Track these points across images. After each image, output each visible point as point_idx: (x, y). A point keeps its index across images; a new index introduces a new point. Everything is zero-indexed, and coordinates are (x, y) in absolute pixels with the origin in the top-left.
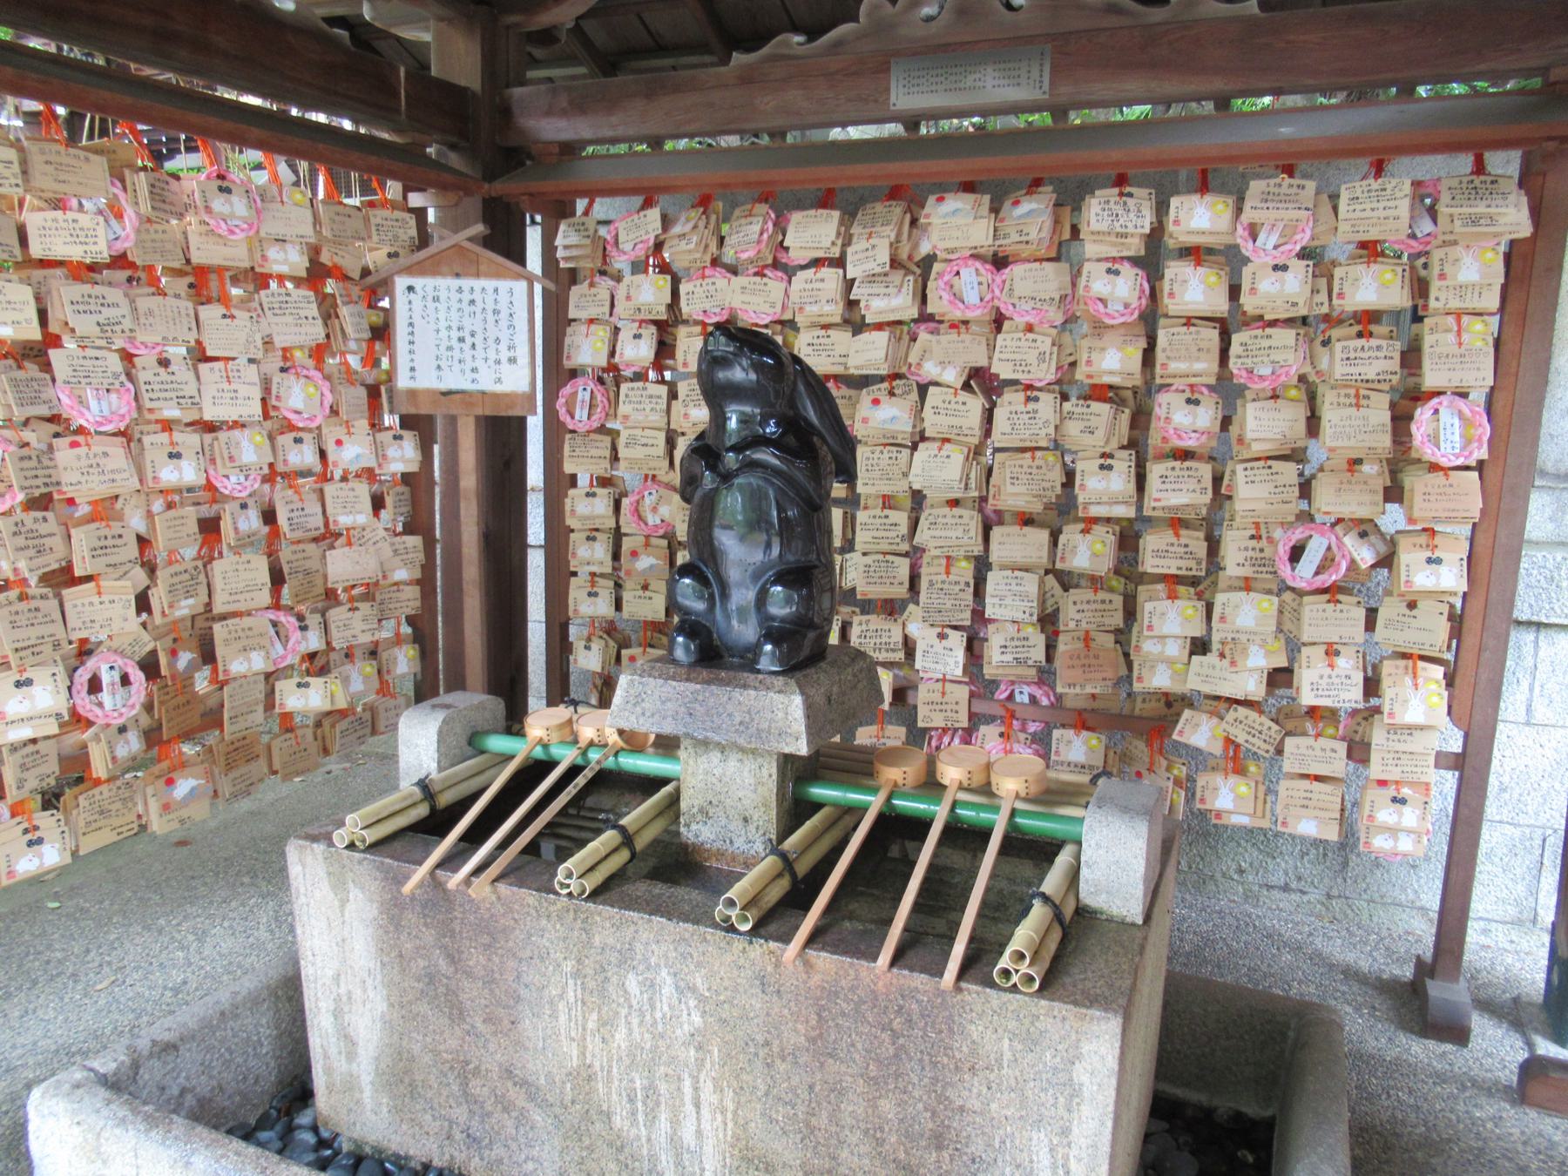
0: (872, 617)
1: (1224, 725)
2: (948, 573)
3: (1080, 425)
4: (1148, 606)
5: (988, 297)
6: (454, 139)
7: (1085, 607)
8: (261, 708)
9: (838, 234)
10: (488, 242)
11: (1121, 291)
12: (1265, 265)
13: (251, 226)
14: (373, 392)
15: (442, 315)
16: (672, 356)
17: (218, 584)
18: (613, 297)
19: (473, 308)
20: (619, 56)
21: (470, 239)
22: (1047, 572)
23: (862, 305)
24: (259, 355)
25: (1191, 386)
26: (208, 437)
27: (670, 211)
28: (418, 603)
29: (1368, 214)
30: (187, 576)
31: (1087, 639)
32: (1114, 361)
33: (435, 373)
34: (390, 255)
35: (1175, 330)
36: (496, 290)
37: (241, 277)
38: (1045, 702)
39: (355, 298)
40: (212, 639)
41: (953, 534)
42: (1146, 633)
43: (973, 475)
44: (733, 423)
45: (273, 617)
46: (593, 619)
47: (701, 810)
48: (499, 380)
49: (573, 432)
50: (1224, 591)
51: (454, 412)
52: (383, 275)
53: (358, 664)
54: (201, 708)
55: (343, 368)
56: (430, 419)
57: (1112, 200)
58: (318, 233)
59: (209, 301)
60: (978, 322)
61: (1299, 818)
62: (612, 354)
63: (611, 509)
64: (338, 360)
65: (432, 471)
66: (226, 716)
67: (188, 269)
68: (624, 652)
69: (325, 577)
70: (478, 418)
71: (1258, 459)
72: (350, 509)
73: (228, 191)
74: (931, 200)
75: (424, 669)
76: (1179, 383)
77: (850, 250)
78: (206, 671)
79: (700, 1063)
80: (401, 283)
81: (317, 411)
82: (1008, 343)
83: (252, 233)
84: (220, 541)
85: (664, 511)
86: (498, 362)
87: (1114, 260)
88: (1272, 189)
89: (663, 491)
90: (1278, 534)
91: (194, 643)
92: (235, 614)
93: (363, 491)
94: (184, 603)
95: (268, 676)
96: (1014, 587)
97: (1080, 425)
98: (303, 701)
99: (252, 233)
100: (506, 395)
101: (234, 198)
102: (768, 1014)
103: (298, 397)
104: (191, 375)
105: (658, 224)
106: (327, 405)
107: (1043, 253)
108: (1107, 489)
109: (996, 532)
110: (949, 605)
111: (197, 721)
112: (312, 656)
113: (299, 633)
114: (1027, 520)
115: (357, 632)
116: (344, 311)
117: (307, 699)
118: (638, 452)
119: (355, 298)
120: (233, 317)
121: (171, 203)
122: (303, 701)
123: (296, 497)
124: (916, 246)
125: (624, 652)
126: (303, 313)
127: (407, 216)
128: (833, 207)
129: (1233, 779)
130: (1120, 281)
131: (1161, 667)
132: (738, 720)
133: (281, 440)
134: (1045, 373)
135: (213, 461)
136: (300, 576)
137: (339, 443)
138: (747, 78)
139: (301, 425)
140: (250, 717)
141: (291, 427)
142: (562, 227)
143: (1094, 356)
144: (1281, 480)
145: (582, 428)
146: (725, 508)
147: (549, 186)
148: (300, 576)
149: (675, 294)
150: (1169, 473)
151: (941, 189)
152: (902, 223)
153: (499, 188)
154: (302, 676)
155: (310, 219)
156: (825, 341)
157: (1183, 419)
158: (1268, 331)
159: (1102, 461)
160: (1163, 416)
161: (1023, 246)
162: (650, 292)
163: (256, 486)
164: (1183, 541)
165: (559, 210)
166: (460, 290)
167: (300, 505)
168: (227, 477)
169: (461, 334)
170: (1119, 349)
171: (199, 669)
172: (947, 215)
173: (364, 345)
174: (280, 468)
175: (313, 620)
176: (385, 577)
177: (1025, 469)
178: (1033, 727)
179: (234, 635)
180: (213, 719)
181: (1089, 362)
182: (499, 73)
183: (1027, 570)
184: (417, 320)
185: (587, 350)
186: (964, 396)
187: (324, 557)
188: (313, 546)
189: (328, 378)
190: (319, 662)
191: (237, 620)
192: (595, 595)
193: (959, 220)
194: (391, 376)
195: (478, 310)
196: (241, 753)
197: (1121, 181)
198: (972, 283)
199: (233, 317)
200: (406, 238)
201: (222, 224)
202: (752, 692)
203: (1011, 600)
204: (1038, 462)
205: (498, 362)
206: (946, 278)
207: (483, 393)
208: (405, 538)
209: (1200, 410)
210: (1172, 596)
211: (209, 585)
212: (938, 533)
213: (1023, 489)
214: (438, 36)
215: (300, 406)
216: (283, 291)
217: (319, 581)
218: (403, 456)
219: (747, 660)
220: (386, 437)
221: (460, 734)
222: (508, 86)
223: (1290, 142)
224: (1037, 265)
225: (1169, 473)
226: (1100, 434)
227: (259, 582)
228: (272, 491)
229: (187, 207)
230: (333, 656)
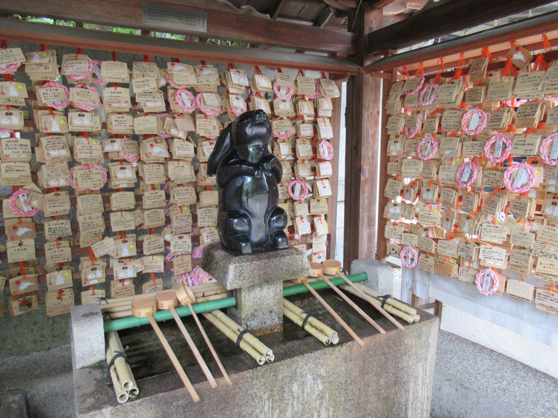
0: (152, 235)
2: (181, 212)
29: (306, 87)
47: (251, 316)
68: (11, 281)
77: (133, 80)
79: (321, 404)
82: (201, 122)
96: (208, 214)
102: (347, 370)
110: (184, 225)
132: (285, 269)
156: (122, 119)
186: (187, 143)
202: (288, 257)
212: (181, 197)
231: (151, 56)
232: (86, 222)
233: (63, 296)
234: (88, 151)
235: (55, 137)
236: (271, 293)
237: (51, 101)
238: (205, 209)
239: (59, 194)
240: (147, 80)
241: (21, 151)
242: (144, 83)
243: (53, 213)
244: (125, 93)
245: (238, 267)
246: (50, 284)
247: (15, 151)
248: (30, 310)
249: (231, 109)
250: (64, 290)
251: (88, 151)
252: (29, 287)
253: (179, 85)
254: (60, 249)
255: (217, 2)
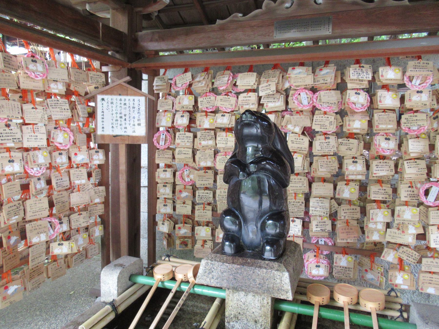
1: (398, 254)
2: (295, 199)
3: (346, 147)
4: (371, 211)
5: (311, 102)
6: (118, 49)
7: (347, 211)
8: (44, 255)
9: (256, 81)
10: (129, 83)
11: (360, 100)
12: (414, 91)
13: (44, 75)
14: (89, 136)
15: (114, 109)
16: (195, 123)
17: (28, 209)
18: (173, 103)
19: (125, 106)
20: (173, 23)
21: (125, 82)
22: (332, 199)
23: (265, 105)
24: (47, 123)
25: (386, 133)
26: (25, 154)
27: (194, 74)
28: (103, 210)
30: (15, 207)
31: (347, 222)
32: (357, 124)
33: (111, 129)
34: (95, 88)
35: (379, 114)
36: (134, 100)
37: (40, 94)
38: (330, 244)
39: (83, 102)
40: (25, 230)
41: (298, 185)
42: (371, 221)
43: (305, 165)
44: (250, 150)
45: (49, 220)
46: (165, 214)
48: (134, 132)
49: (158, 149)
50: (398, 206)
51: (117, 143)
52: (93, 94)
53: (81, 234)
54: (20, 256)
55: (78, 127)
56: (108, 145)
57: (357, 68)
58: (70, 79)
59: (27, 102)
60: (306, 111)
61: (427, 288)
62: (173, 122)
63: (172, 176)
64: (76, 124)
65: (109, 162)
66: (30, 260)
67: (19, 90)
68: (176, 226)
69: (70, 203)
70: (126, 144)
71: (411, 159)
72: (80, 179)
73: (35, 61)
74: (290, 69)
75: (105, 233)
76: (382, 133)
77: (260, 86)
78: (23, 242)
80: (99, 97)
81: (67, 143)
82: (318, 118)
83: (44, 77)
84: (29, 192)
85: (192, 176)
86: (134, 125)
87: (357, 89)
88: (417, 65)
89: (191, 170)
90: (419, 185)
91: (18, 232)
92: (35, 220)
93: (84, 171)
94: (13, 218)
95: (47, 242)
96: (320, 204)
97: (346, 147)
98: (60, 250)
99: (44, 77)
100: (137, 137)
101: (38, 65)
103: (61, 138)
104: (19, 131)
105: (191, 77)
106: (71, 141)
107: (331, 87)
108: (354, 170)
109: (314, 185)
110: (296, 210)
111: (18, 262)
112: (64, 233)
113: (59, 226)
114: (324, 180)
115: (81, 222)
116: (79, 107)
117: (61, 249)
118: (182, 156)
119: (83, 102)
120: (36, 108)
121: (13, 65)
122: (60, 250)
123: (59, 175)
124: (283, 85)
125: (176, 226)
126: (63, 107)
127: (102, 74)
128: (254, 72)
129: (402, 273)
130: (360, 96)
131: (375, 233)
132: (258, 282)
133: (54, 154)
134: (333, 129)
135: (27, 163)
136: (60, 204)
137: (76, 154)
138: (222, 28)
139: (62, 148)
140: (40, 259)
141: (58, 149)
142: (156, 79)
143: (351, 123)
144: (420, 167)
145: (162, 148)
146: (244, 186)
147: (152, 64)
148: (60, 204)
149: (196, 101)
150: (379, 164)
151: (294, 66)
152: (280, 76)
153: (134, 65)
154: (60, 241)
155: (67, 73)
157: (385, 146)
158: (415, 114)
159: (353, 160)
160: (378, 144)
161: (324, 85)
162: (187, 101)
163: (44, 171)
164: (384, 188)
165: (154, 73)
166: (121, 100)
167: (60, 178)
168: (33, 169)
169: (121, 115)
170: (360, 120)
171: (20, 242)
172: (296, 74)
173: (85, 119)
174: (53, 164)
175: (65, 220)
176: (91, 202)
177: (325, 162)
178: (325, 253)
179: (34, 228)
180: (25, 260)
181: (349, 125)
182: (133, 27)
183: (324, 198)
184: (105, 111)
185: (164, 121)
186: (302, 137)
187: (69, 196)
188: (65, 192)
189: (72, 131)
190: (67, 235)
191: (35, 222)
192: (166, 205)
193: (302, 76)
194: (95, 130)
195: (127, 107)
196: (37, 271)
197: (358, 62)
198: (305, 98)
199: (36, 108)
200: (101, 82)
201: (33, 74)
202: (265, 270)
203: (318, 208)
204: (329, 160)
205: (134, 125)
206: (296, 96)
207: (129, 136)
208: (99, 187)
209: (390, 142)
210: (379, 208)
211: (24, 210)
213: (325, 170)
214: (113, 16)
215: (61, 141)
216: (56, 99)
217: (67, 204)
218: (99, 158)
219: (257, 254)
220: (93, 152)
221: (127, 276)
222: (136, 32)
223: (424, 47)
224: (328, 91)
225: (379, 164)
226: (354, 150)
227: (44, 207)
228: (50, 172)
229: (19, 67)
230: (72, 231)
231: (306, 62)
232: (221, 194)
233: (205, 245)
234: (225, 142)
235: (207, 131)
236: (256, 302)
237: (205, 106)
238: (318, 199)
239: (207, 172)
240: (269, 85)
241: (186, 141)
242: (267, 87)
243: (202, 185)
244: (253, 97)
245: (209, 264)
246: (197, 234)
247: (183, 140)
248: (186, 248)
249: (348, 105)
250: (208, 241)
251: (225, 142)
252: (185, 233)
253: (298, 86)
254: (205, 211)
255: (345, 3)
